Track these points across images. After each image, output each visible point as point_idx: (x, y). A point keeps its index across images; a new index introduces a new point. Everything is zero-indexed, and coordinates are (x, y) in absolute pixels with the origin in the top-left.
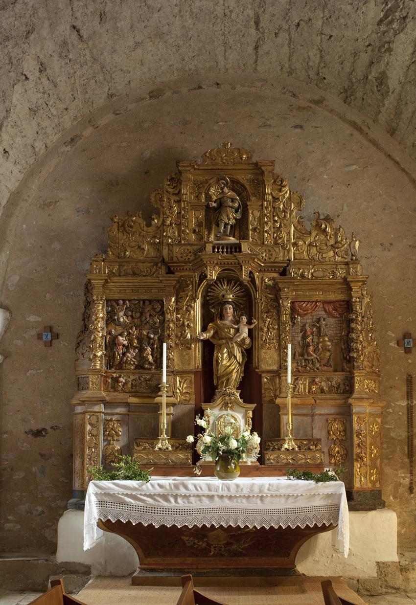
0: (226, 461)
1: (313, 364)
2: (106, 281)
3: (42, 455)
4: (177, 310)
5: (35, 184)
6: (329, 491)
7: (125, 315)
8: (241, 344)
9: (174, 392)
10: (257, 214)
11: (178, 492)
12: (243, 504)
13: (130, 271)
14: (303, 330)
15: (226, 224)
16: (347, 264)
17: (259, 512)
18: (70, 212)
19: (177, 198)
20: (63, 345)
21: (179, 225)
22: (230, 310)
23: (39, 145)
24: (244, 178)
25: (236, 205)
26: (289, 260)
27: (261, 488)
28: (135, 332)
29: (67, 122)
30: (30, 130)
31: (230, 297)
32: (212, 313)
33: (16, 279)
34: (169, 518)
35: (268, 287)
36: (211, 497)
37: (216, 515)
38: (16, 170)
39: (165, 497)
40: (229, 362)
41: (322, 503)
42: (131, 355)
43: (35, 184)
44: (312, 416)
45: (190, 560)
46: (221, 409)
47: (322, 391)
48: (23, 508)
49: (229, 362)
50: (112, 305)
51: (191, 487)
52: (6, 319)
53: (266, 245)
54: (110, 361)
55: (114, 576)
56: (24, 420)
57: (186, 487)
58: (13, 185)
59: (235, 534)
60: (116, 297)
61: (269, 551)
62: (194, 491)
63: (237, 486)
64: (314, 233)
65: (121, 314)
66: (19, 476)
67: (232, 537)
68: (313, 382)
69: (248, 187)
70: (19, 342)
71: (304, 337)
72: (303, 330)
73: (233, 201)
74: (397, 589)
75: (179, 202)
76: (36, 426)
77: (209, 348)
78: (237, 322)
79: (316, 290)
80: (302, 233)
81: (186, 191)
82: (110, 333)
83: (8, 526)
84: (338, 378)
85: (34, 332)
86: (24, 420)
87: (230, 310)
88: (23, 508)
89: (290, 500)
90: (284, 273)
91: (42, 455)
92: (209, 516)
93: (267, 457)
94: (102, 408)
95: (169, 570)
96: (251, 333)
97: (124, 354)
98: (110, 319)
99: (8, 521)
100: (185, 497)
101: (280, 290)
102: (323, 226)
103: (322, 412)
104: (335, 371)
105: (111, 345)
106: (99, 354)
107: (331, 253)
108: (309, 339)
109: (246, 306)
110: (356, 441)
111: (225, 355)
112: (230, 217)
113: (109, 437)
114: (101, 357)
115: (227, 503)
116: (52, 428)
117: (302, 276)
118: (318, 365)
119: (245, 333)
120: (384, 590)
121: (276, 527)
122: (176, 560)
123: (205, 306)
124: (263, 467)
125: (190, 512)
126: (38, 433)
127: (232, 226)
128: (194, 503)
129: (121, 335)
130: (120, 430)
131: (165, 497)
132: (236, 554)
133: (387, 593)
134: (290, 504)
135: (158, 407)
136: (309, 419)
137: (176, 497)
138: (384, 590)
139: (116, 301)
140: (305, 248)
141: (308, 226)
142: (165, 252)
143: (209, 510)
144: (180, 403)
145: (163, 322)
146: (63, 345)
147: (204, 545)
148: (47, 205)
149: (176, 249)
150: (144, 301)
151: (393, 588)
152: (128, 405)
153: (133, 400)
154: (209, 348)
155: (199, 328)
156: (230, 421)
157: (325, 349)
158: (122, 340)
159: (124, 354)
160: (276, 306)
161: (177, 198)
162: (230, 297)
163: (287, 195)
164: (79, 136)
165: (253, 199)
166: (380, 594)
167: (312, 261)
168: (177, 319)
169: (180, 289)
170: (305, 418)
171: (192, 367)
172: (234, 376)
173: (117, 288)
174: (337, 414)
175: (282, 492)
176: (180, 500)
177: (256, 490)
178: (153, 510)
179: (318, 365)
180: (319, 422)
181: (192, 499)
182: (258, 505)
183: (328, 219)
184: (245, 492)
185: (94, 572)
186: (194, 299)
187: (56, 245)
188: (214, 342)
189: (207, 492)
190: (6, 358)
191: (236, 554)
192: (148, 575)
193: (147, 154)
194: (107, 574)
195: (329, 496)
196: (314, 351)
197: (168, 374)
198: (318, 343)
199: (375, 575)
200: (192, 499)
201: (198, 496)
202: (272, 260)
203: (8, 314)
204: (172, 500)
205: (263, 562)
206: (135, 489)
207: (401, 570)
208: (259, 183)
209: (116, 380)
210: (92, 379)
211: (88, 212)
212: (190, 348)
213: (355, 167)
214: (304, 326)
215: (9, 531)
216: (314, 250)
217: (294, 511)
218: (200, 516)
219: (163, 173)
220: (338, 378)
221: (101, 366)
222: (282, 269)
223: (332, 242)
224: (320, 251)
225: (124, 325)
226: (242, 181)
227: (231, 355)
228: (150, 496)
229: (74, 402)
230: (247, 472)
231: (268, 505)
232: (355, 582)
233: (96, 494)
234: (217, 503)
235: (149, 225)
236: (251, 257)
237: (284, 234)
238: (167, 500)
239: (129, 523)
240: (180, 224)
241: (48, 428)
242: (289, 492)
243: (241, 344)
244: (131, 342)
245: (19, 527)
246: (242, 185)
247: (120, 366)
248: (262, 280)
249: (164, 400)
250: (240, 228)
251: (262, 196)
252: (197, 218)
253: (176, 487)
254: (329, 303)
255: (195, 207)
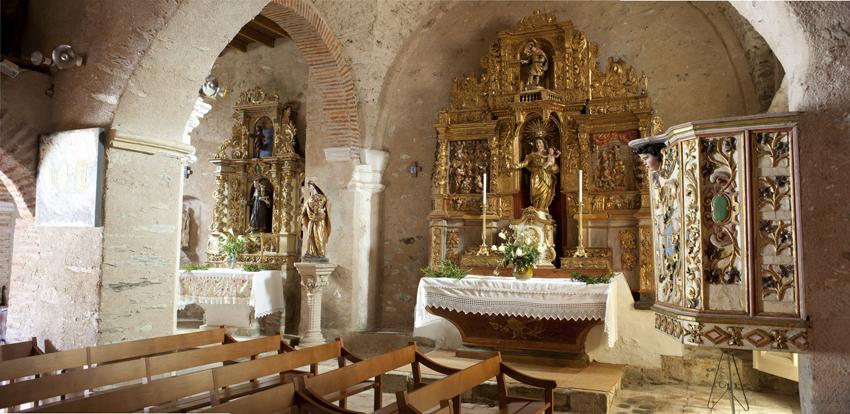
0: (520, 265)
1: (608, 184)
2: (447, 128)
3: (411, 258)
4: (499, 147)
5: (404, 60)
6: (597, 291)
7: (463, 152)
8: (549, 171)
9: (493, 209)
10: (561, 64)
11: (482, 288)
12: (529, 299)
13: (466, 119)
14: (601, 157)
15: (535, 77)
16: (636, 98)
17: (541, 306)
18: (429, 77)
19: (498, 60)
20: (425, 175)
21: (500, 80)
22: (540, 144)
23: (405, 32)
24: (550, 37)
25: (543, 60)
26: (588, 100)
27: (542, 286)
28: (470, 164)
29: (424, 11)
30: (395, 24)
31: (541, 133)
32: (527, 148)
33: (393, 128)
34: (475, 307)
35: (569, 123)
36: (505, 293)
37: (541, 310)
38: (389, 52)
39: (472, 291)
40: (542, 185)
41: (591, 301)
42: (467, 182)
43: (404, 60)
44: (607, 228)
45: (498, 341)
46: (526, 224)
47: (616, 207)
48: (398, 296)
49: (542, 185)
50: (453, 143)
51: (490, 284)
52: (386, 158)
53: (569, 90)
54: (455, 189)
55: (449, 350)
56: (399, 232)
57: (487, 285)
58: (388, 63)
59: (528, 323)
60: (456, 139)
61: (566, 338)
62: (492, 288)
63: (525, 285)
64: (609, 75)
65: (460, 151)
66: (396, 272)
67: (527, 325)
68: (608, 200)
69: (553, 44)
70: (396, 175)
71: (602, 163)
72: (601, 157)
73: (540, 57)
74: (680, 381)
75: (500, 62)
76: (407, 236)
77: (526, 175)
78: (547, 153)
79: (609, 122)
80: (598, 77)
81: (506, 54)
82: (452, 166)
83: (388, 308)
84: (629, 196)
85: (405, 167)
86: (399, 232)
87: (540, 144)
88: (398, 296)
89: (566, 298)
90: (584, 111)
91: (411, 258)
92: (504, 307)
93: (562, 262)
94: (445, 223)
95: (484, 348)
96: (558, 161)
97: (462, 182)
98: (453, 156)
99: (388, 305)
100: (486, 292)
101: (578, 125)
102: (616, 68)
103: (616, 225)
104: (629, 190)
105: (453, 175)
106: (443, 183)
107: (624, 91)
108: (606, 165)
109: (554, 139)
110: (642, 248)
111: (537, 180)
112: (538, 71)
113: (449, 244)
114: (445, 184)
115: (517, 298)
116: (418, 237)
117: (599, 112)
118: (613, 185)
119: (552, 161)
120: (667, 380)
121: (555, 319)
122: (489, 340)
123: (523, 141)
124: (557, 268)
125: (489, 303)
126: (408, 241)
127: (540, 77)
128: (493, 297)
129: (459, 167)
130: (458, 240)
131: (472, 291)
132: (533, 339)
133: (669, 383)
134: (565, 301)
135: (480, 223)
136: (605, 231)
137: (480, 291)
138: (667, 380)
139: (456, 142)
140: (601, 88)
141: (604, 70)
142: (491, 102)
143: (505, 303)
144: (502, 219)
145: (489, 156)
146: (425, 175)
147: (508, 330)
148: (413, 73)
149: (498, 99)
150: (476, 140)
151: (677, 380)
152: (464, 220)
153: (467, 217)
154: (526, 175)
155: (517, 158)
156: (536, 235)
157: (619, 172)
158: (461, 171)
159: (462, 182)
160: (574, 139)
161: (498, 60)
162: (541, 133)
163: (585, 46)
164: (434, 20)
165: (557, 52)
166: (662, 384)
167: (608, 100)
168: (500, 154)
169: (501, 130)
170: (601, 230)
171: (511, 190)
172: (545, 195)
173: (457, 131)
174: (628, 226)
175: (560, 291)
176: (482, 294)
177: (539, 288)
178: (463, 300)
179: (613, 185)
180: (613, 234)
181: (491, 294)
182: (541, 300)
183: (620, 62)
184: (531, 290)
185: (437, 346)
186: (512, 137)
187: (420, 102)
188: (530, 169)
189: (501, 289)
190: (387, 186)
191: (533, 339)
192: (468, 350)
193: (483, 26)
194: (446, 348)
195: (597, 296)
196: (611, 173)
197: (181, 320)
198: (614, 167)
199: (660, 367)
200: (491, 294)
201: (496, 292)
202: (574, 100)
203: (387, 155)
204: (477, 293)
205: (554, 347)
206: (451, 285)
207: (685, 364)
208: (561, 40)
209: (456, 202)
210: (438, 202)
211: (441, 75)
212: (509, 176)
213: (652, 11)
214: (601, 153)
215: (388, 312)
216: (609, 90)
217: (569, 306)
218: (497, 307)
219: (489, 40)
220: (629, 196)
221: (445, 192)
222: (581, 108)
223: (624, 81)
224: (614, 89)
225: (463, 160)
226: (548, 39)
227: (541, 179)
228: (461, 290)
229: (428, 219)
230: (541, 273)
231: (548, 301)
232: (640, 371)
233: (425, 288)
234: (510, 298)
235: (479, 82)
236: (550, 103)
237: (583, 79)
238: (474, 294)
239: (447, 309)
240: (503, 74)
241: (414, 237)
242: (564, 291)
243: (549, 171)
244: (467, 172)
245: (395, 309)
246: (549, 43)
247: (459, 191)
248: (565, 118)
249: (484, 217)
250: (547, 79)
251: (563, 49)
252: (514, 73)
253: (480, 284)
254: (622, 132)
255: (512, 65)
